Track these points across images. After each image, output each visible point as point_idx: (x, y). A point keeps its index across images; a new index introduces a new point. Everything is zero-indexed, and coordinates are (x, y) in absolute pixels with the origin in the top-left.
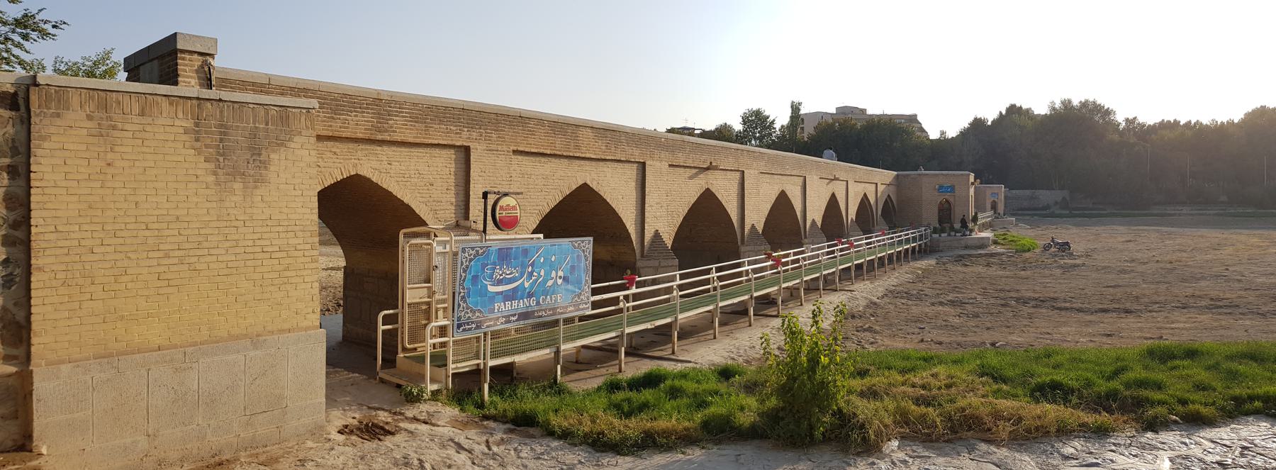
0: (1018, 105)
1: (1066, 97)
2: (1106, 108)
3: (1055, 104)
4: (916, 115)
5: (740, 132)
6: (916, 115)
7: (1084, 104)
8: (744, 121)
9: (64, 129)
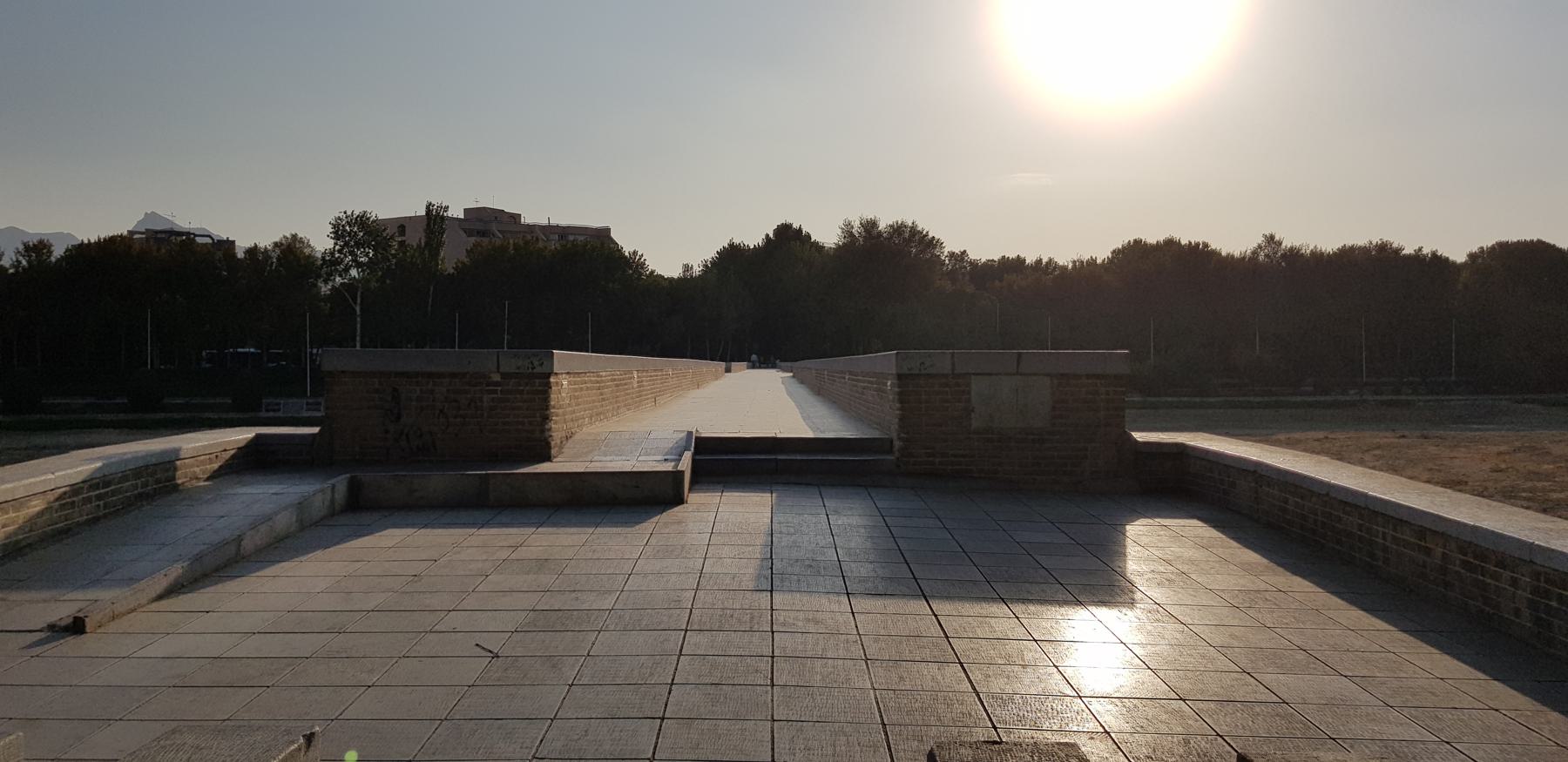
0: (795, 226)
1: (869, 216)
2: (930, 236)
3: (852, 227)
4: (607, 230)
5: (332, 254)
6: (607, 230)
7: (898, 229)
8: (336, 233)
9: (856, 641)
